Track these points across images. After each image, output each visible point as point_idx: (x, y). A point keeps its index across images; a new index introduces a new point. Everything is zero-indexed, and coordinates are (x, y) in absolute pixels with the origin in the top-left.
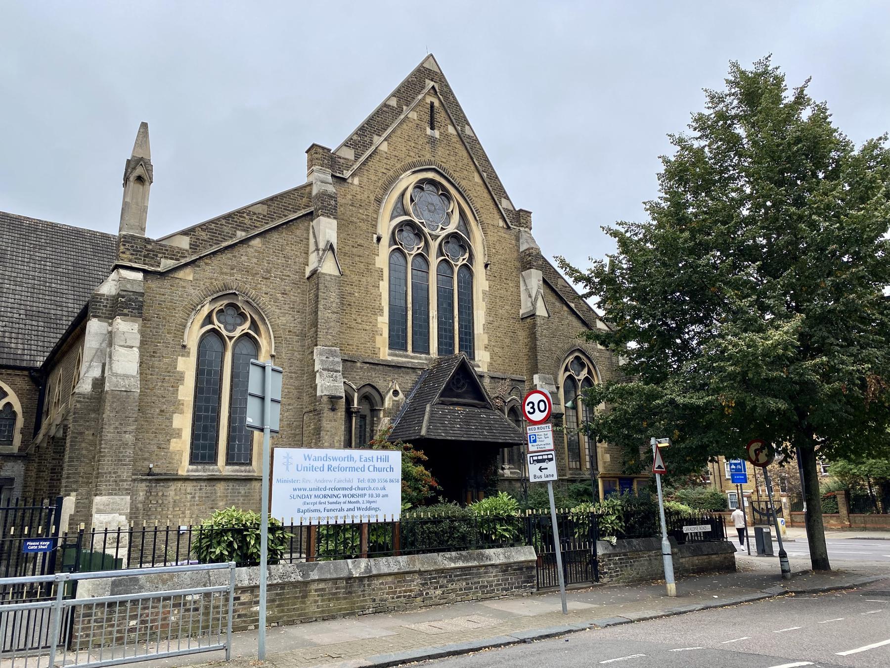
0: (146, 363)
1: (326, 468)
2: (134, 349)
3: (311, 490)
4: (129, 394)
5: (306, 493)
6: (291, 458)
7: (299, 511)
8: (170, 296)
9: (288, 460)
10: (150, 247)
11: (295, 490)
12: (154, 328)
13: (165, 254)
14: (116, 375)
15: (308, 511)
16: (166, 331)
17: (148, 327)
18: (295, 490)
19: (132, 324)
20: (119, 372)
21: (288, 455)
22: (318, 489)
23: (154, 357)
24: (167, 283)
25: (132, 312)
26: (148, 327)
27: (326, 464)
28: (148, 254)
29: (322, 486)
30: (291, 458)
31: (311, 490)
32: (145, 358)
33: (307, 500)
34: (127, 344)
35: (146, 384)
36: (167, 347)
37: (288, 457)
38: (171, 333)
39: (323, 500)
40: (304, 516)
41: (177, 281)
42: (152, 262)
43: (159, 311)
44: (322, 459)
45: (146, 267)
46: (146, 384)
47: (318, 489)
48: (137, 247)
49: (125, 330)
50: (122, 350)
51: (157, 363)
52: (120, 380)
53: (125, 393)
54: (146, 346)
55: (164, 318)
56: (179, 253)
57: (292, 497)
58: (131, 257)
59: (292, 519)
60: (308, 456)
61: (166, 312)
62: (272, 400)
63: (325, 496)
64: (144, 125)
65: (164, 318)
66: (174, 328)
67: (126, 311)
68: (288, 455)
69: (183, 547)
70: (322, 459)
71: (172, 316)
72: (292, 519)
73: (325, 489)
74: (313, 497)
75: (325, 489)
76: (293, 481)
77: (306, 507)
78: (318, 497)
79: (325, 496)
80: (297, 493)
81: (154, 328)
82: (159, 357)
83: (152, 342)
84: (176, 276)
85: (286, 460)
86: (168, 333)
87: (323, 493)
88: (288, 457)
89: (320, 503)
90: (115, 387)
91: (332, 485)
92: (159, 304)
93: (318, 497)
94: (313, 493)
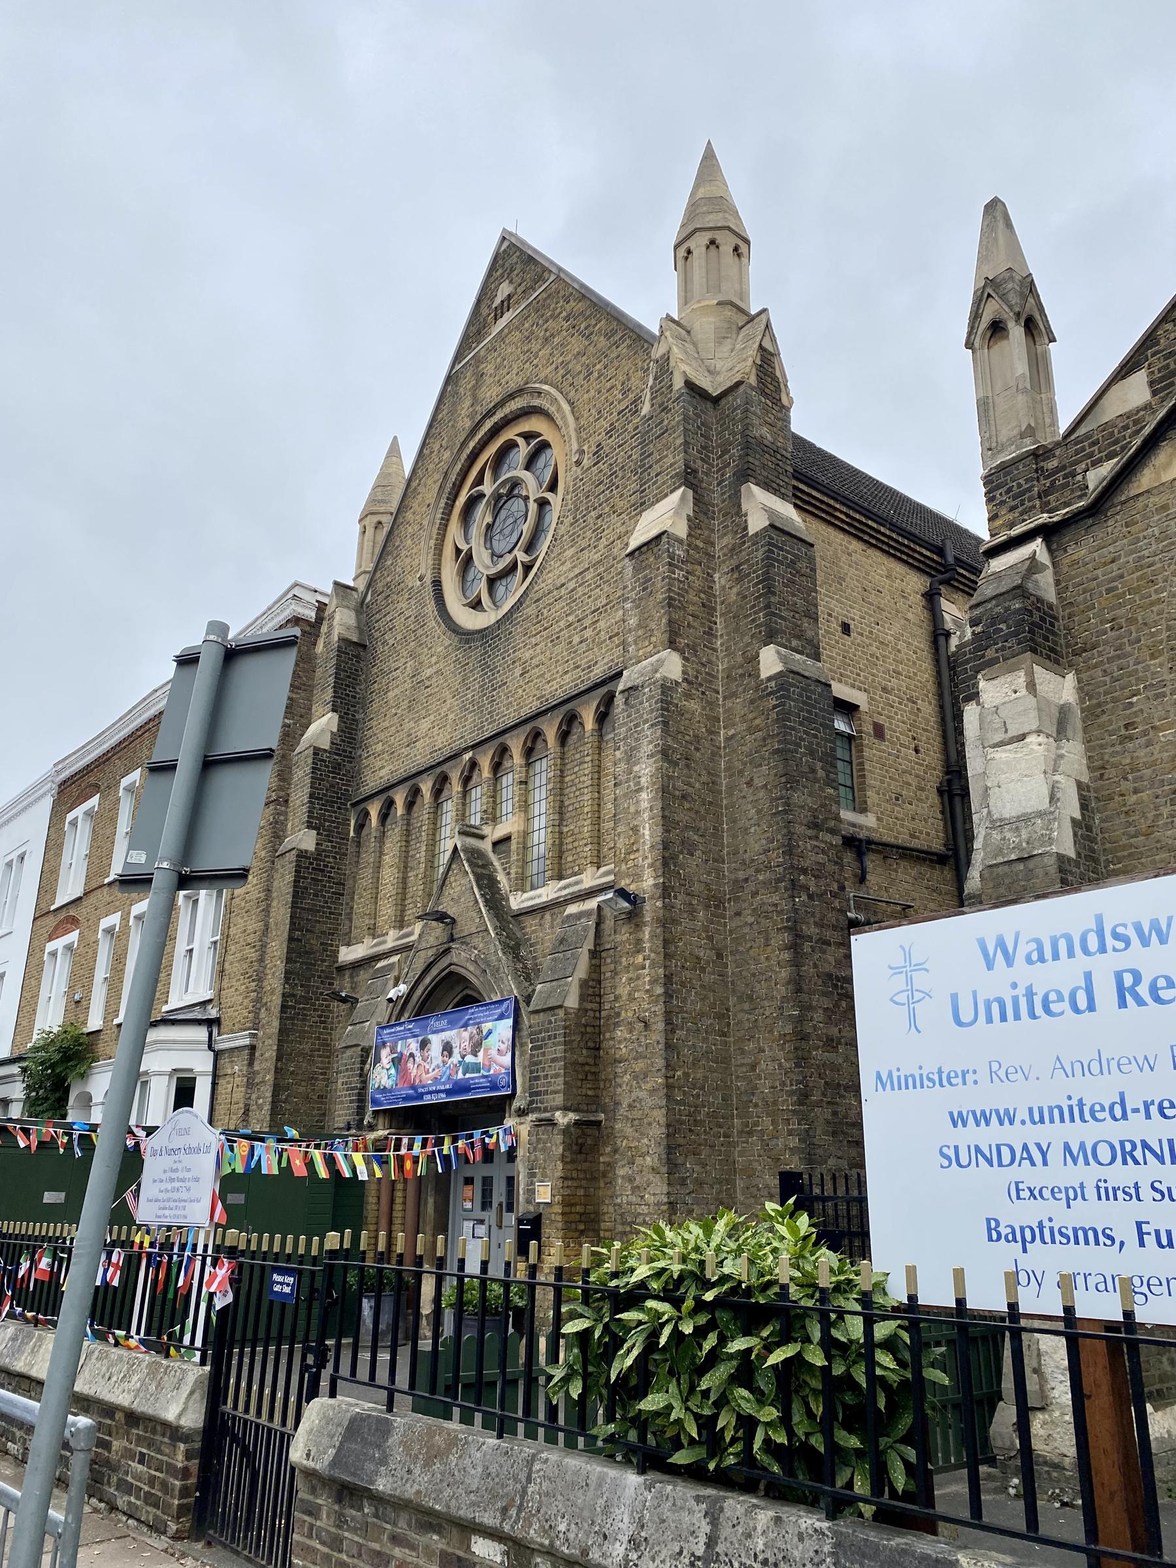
0: (1115, 766)
1: (1106, 993)
2: (1031, 739)
3: (1039, 1117)
4: (1031, 864)
5: (1017, 1135)
6: (920, 967)
7: (993, 1231)
8: (1132, 552)
9: (910, 981)
10: (1053, 464)
11: (958, 1120)
12: (1110, 660)
13: (1091, 455)
14: (998, 824)
15: (1039, 1233)
16: (1146, 653)
17: (1095, 666)
18: (958, 1120)
19: (1008, 678)
20: (1006, 815)
21: (908, 956)
22: (1077, 1112)
23: (1131, 738)
24: (1113, 525)
25: (1003, 649)
26: (1095, 666)
27: (1104, 968)
28: (1053, 483)
29: (1099, 1091)
30: (920, 967)
31: (1039, 1117)
32: (1109, 750)
33: (1030, 1176)
34: (1010, 734)
35: (1130, 824)
36: (1157, 696)
37: (909, 967)
38: (1161, 653)
39: (1121, 1175)
40: (1026, 1263)
41: (1140, 504)
42: (1067, 495)
43: (1112, 609)
44: (1077, 946)
45: (1044, 518)
46: (1130, 824)
47: (1077, 1112)
48: (1020, 486)
49: (997, 702)
50: (1002, 755)
51: (1141, 753)
52: (1008, 835)
53: (1021, 866)
54: (1104, 718)
55: (1132, 621)
56: (1126, 428)
57: (952, 1158)
58: (1011, 516)
59: (959, 1275)
60: (1001, 944)
61: (1133, 601)
62: (1006, 731)
63: (1126, 1153)
64: (994, 208)
65: (1132, 621)
66: (1164, 635)
67: (990, 653)
68: (908, 956)
69: (425, 1338)
70: (1077, 946)
71: (1152, 604)
72: (959, 1275)
73: (1120, 1110)
74: (1056, 1154)
75: (1120, 1110)
76: (943, 1079)
77: (1027, 1213)
78: (1087, 1154)
79: (1126, 1153)
80: (972, 1135)
81: (1110, 660)
82: (1145, 733)
83: (1115, 700)
84: (1133, 492)
85: (900, 982)
86: (1153, 657)
87: (1115, 1132)
88: (909, 967)
89: (1107, 1193)
90: (995, 857)
91: (1055, 1092)
92: (1108, 591)
93: (1087, 1154)
94: (1055, 1134)
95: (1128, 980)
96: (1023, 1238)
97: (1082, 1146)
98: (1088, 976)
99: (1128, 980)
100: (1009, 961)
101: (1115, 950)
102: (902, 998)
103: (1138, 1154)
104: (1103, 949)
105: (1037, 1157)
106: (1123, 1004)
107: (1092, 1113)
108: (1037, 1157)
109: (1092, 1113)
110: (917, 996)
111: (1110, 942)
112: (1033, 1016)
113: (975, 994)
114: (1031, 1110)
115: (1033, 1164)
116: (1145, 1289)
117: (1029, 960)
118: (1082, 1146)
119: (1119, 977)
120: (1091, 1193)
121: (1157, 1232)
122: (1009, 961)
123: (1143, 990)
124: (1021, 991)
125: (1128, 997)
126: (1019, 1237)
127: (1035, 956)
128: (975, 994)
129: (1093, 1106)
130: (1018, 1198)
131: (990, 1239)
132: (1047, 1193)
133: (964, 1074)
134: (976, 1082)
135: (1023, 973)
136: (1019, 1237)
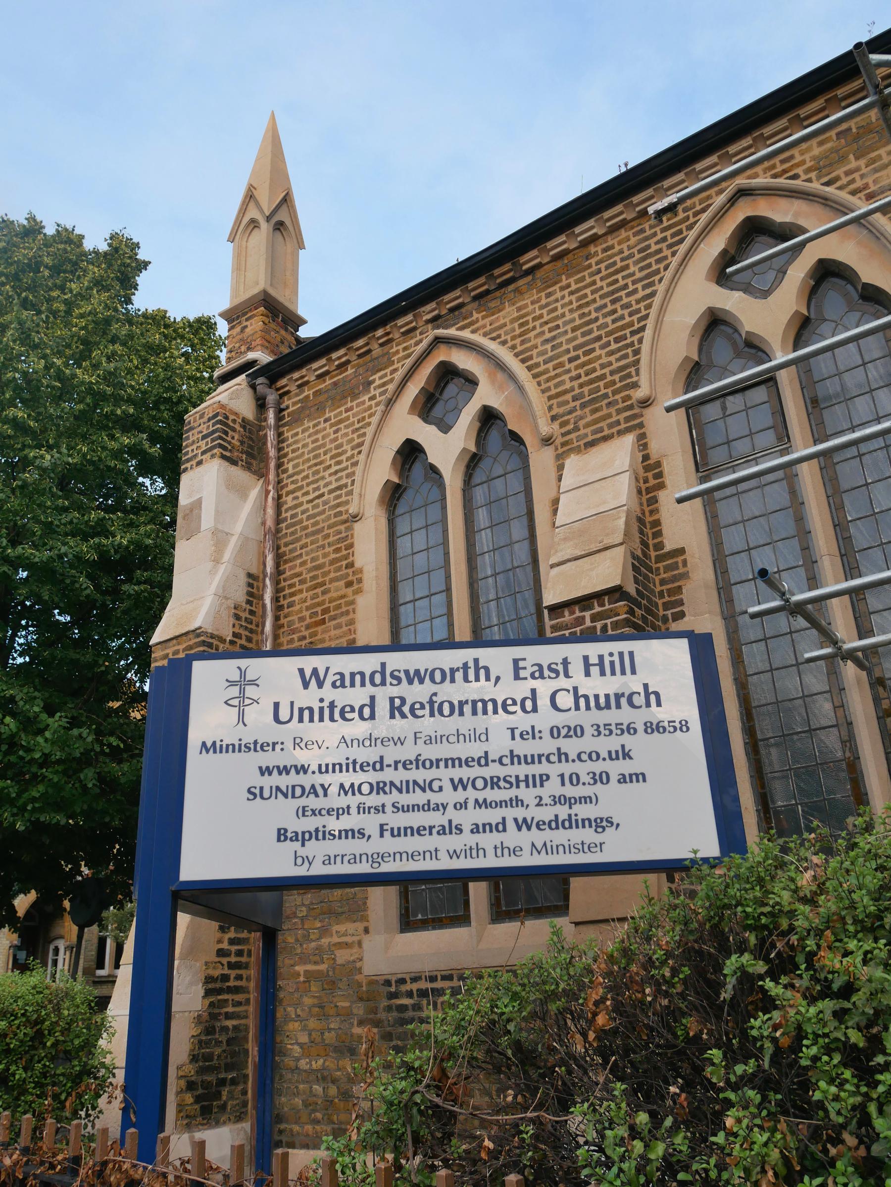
1: (383, 708)
18: (265, 771)
30: (253, 683)
33: (312, 802)
39: (374, 800)
75: (380, 765)
80: (276, 780)
85: (235, 691)
93: (355, 789)
95: (397, 702)
96: (302, 838)
97: (352, 785)
98: (372, 698)
99: (397, 702)
100: (320, 685)
101: (391, 684)
102: (235, 702)
103: (387, 789)
104: (383, 683)
105: (320, 791)
106: (392, 716)
107: (342, 713)
108: (320, 791)
109: (342, 713)
110: (247, 702)
111: (389, 679)
112: (332, 719)
113: (292, 703)
114: (320, 766)
115: (317, 796)
116: (380, 860)
117: (334, 685)
118: (352, 785)
119: (392, 700)
120: (353, 810)
121: (392, 829)
122: (320, 685)
123: (406, 709)
124: (326, 704)
125: (396, 713)
126: (300, 838)
127: (338, 683)
128: (292, 703)
129: (344, 708)
130: (304, 815)
131: (279, 840)
132: (324, 812)
133: (274, 744)
134: (282, 749)
135: (329, 693)
136: (300, 838)
